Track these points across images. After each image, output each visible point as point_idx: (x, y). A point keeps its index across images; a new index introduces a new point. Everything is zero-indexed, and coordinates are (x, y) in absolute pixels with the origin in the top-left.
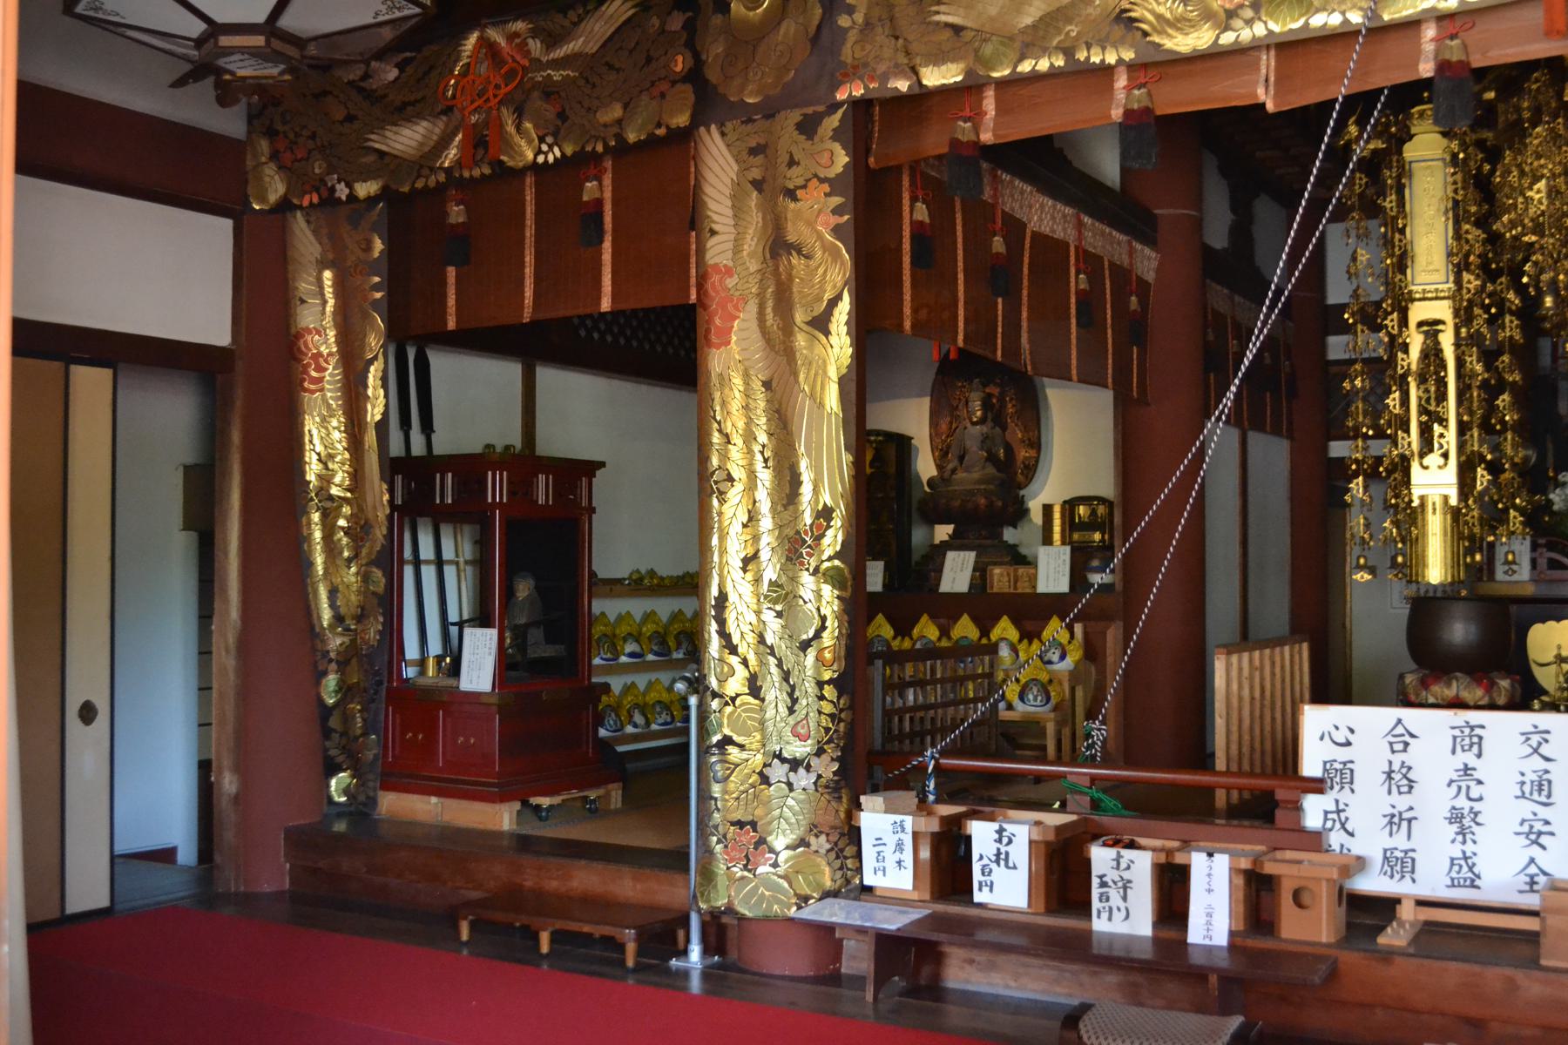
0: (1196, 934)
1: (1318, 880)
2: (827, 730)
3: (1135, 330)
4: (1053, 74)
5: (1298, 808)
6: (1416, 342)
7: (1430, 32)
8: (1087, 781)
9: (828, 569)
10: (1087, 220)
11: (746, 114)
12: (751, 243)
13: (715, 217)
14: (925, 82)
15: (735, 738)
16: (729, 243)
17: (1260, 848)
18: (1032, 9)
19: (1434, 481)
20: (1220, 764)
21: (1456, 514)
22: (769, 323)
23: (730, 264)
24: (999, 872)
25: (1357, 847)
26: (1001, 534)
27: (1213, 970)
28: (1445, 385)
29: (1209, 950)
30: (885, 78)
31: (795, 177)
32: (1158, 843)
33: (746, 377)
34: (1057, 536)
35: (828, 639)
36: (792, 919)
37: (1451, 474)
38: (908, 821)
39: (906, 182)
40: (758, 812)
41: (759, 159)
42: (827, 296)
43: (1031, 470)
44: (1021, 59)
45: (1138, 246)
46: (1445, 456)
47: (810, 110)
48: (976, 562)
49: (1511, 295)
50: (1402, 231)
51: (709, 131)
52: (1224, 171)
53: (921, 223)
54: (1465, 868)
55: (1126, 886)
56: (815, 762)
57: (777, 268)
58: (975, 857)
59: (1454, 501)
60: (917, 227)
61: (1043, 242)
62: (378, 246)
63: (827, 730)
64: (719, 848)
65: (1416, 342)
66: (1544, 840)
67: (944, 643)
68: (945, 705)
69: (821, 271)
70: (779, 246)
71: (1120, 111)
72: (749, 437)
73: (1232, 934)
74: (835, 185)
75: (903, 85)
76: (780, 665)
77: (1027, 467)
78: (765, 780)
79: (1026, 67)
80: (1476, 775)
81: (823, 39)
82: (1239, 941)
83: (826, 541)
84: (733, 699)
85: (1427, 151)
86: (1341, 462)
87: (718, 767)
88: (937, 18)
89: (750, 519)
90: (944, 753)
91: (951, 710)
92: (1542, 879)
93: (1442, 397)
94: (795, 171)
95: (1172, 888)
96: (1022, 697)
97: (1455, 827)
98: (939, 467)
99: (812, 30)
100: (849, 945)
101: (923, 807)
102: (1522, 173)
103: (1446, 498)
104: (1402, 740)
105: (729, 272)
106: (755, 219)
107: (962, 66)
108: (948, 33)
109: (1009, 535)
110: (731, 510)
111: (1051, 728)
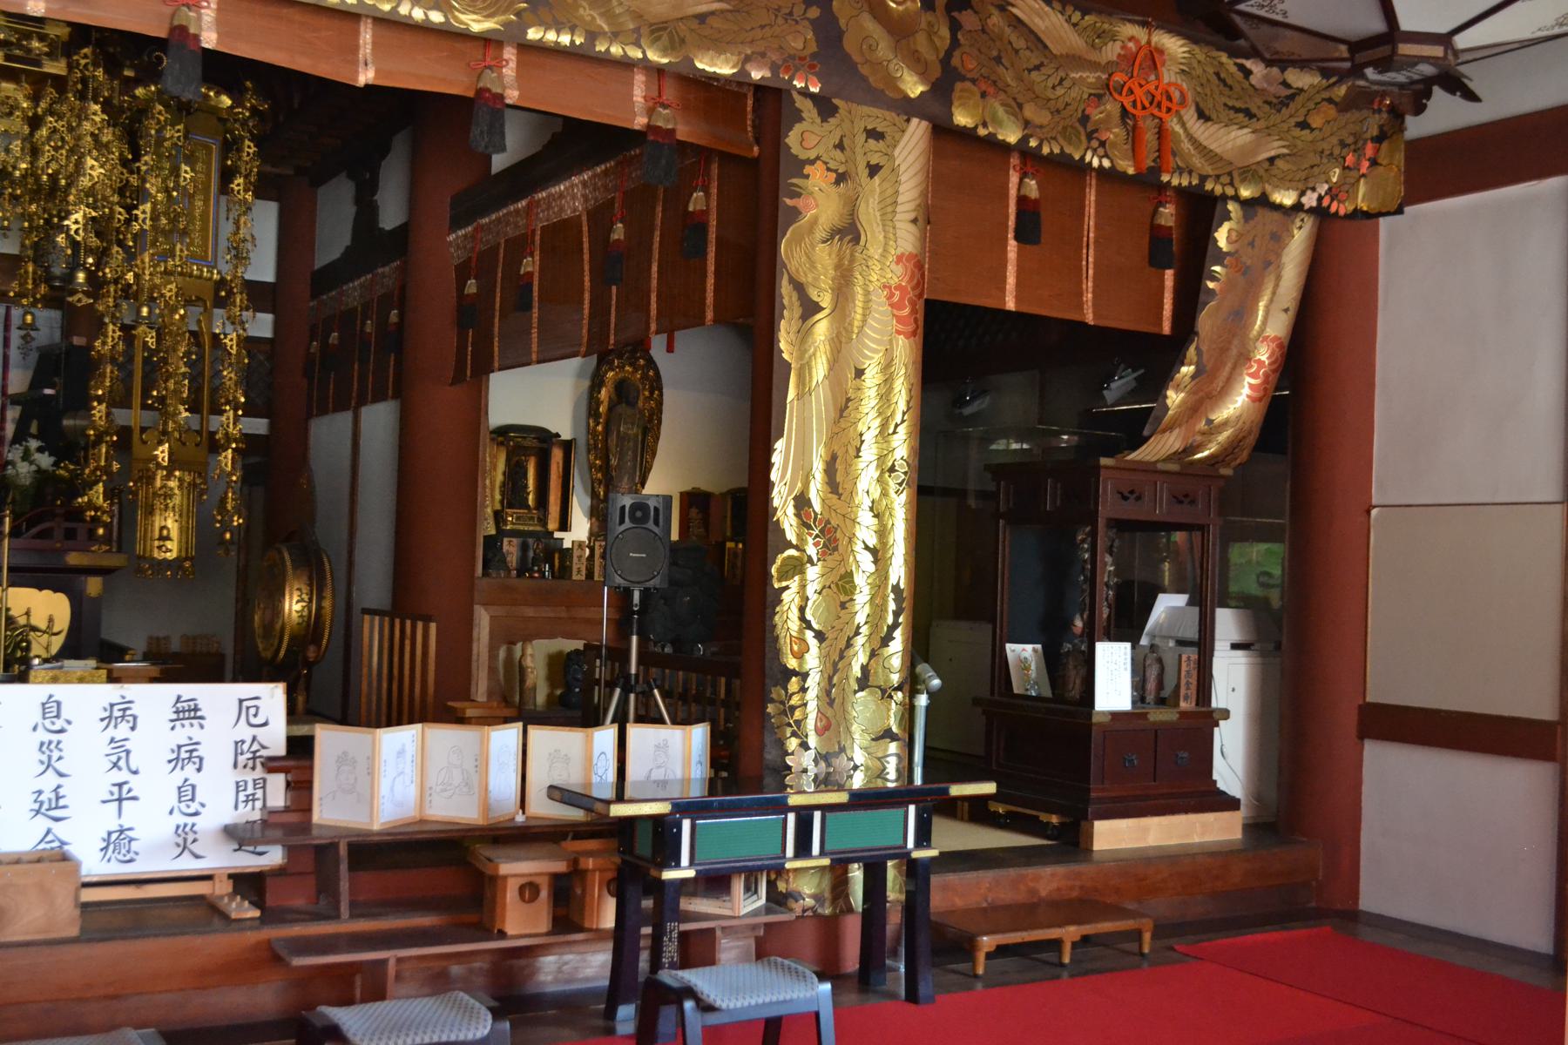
54: (118, 840)
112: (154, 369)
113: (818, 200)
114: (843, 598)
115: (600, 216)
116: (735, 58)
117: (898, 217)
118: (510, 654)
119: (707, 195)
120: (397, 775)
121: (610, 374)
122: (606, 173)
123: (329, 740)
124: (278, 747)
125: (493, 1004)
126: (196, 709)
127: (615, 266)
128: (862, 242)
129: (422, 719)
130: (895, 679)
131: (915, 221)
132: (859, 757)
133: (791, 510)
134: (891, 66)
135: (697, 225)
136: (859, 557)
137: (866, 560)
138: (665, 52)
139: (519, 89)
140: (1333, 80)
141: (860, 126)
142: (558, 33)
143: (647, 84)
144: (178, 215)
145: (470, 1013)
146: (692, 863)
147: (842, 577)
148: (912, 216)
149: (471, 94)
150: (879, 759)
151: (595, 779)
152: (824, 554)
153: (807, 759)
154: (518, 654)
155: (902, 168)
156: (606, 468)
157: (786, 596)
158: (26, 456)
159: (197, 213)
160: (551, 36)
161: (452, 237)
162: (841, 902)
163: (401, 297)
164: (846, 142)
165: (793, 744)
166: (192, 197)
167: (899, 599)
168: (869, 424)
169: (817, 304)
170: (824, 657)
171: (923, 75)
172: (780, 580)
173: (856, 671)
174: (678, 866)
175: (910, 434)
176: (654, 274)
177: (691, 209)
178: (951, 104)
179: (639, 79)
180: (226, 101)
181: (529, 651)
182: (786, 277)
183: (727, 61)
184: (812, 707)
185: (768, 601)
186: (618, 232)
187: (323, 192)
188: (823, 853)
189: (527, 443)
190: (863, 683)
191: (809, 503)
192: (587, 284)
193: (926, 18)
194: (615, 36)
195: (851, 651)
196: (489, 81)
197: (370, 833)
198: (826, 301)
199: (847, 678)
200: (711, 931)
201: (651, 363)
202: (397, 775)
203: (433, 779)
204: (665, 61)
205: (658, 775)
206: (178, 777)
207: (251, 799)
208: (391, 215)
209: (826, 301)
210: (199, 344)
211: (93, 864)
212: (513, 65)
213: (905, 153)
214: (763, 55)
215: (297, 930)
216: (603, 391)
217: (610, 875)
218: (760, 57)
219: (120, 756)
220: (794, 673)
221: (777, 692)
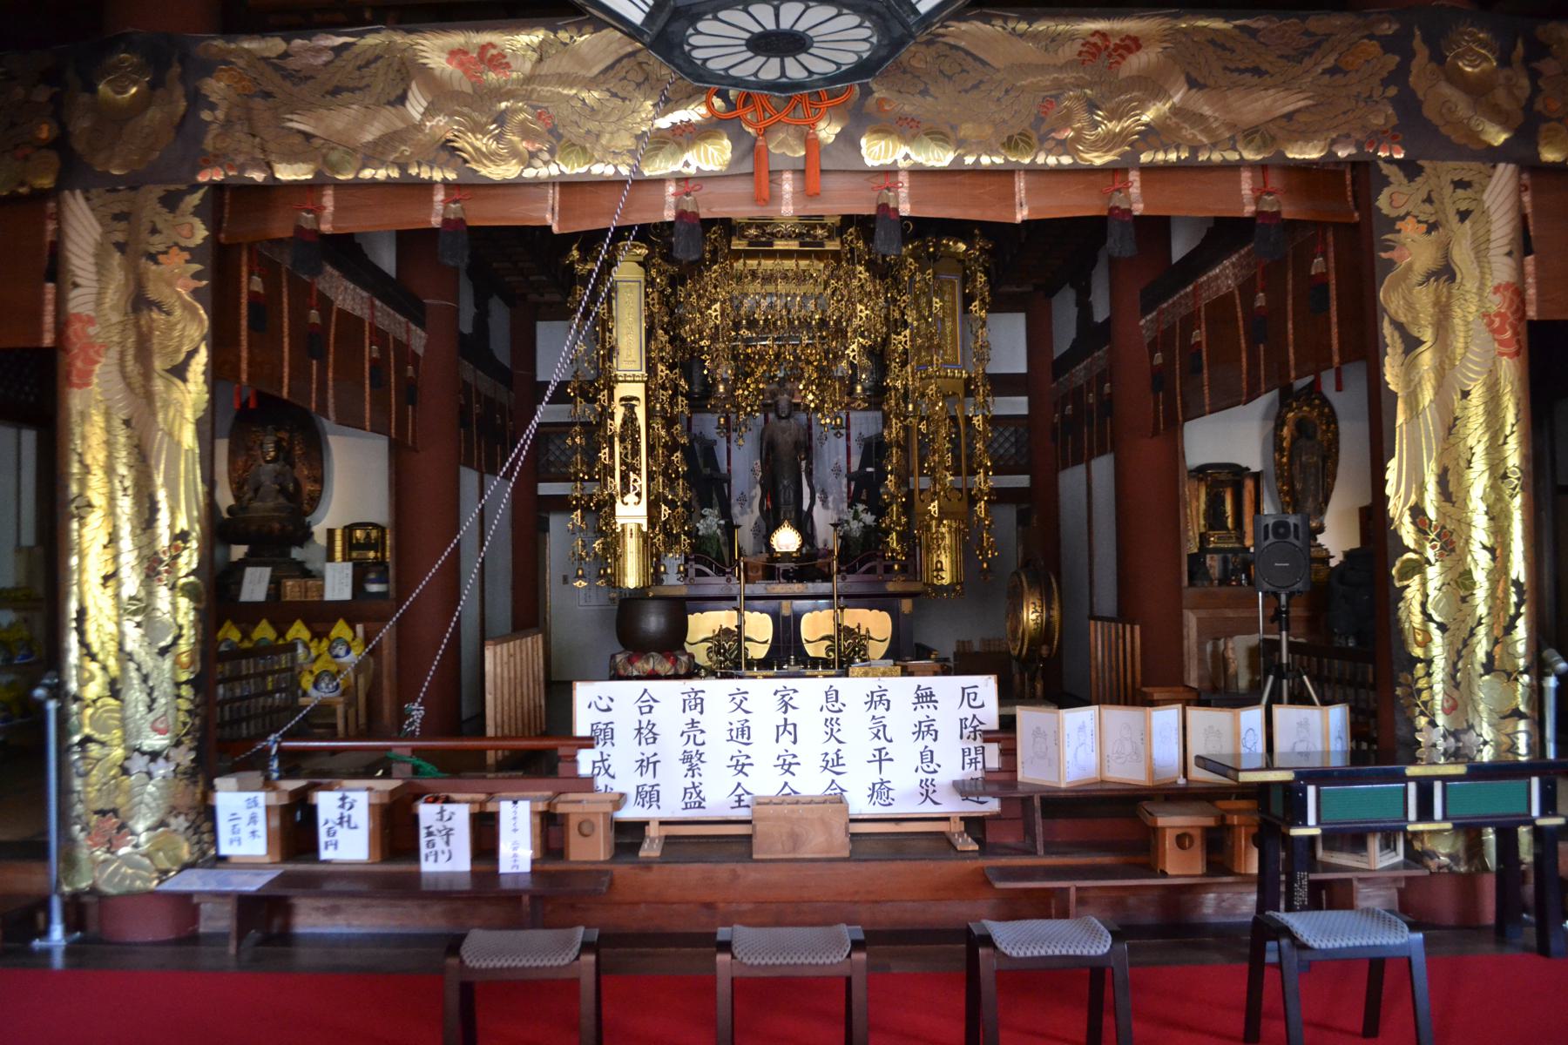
0: (505, 866)
1: (597, 814)
2: (185, 724)
3: (410, 392)
4: (388, 184)
5: (573, 760)
6: (619, 412)
7: (671, 189)
8: (408, 752)
9: (185, 585)
10: (378, 303)
11: (112, 184)
12: (112, 296)
14: (278, 176)
15: (97, 736)
16: (92, 292)
17: (549, 793)
18: (373, 129)
20: (490, 731)
21: (646, 539)
22: (129, 369)
23: (93, 314)
24: (343, 833)
25: (618, 786)
26: (289, 554)
27: (524, 891)
28: (638, 444)
29: (516, 876)
30: (242, 168)
31: (157, 244)
32: (468, 796)
33: (108, 416)
34: (338, 555)
35: (184, 646)
36: (153, 893)
38: (261, 797)
39: (245, 258)
40: (120, 800)
41: (123, 225)
42: (185, 349)
43: (315, 501)
44: (364, 167)
45: (413, 327)
46: (639, 495)
47: (172, 187)
48: (272, 576)
49: (682, 382)
50: (610, 331)
53: (257, 293)
54: (694, 796)
55: (448, 833)
56: (173, 753)
58: (321, 821)
59: (645, 529)
60: (253, 295)
61: (343, 314)
63: (185, 724)
64: (82, 836)
65: (619, 412)
66: (746, 769)
67: (247, 644)
68: (257, 695)
69: (179, 327)
70: (140, 302)
71: (439, 219)
72: (110, 470)
73: (533, 862)
74: (195, 254)
75: (258, 176)
76: (139, 669)
77: (312, 499)
78: (125, 771)
79: (367, 174)
80: (700, 726)
81: (187, 128)
82: (538, 866)
83: (182, 561)
84: (94, 701)
85: (628, 273)
87: (80, 763)
88: (290, 124)
89: (110, 541)
90: (285, 737)
91: (261, 700)
92: (745, 797)
93: (636, 452)
94: (156, 239)
95: (485, 831)
96: (316, 685)
97: (687, 766)
98: (237, 497)
99: (177, 119)
100: (206, 908)
101: (268, 785)
102: (700, 297)
103: (639, 526)
104: (648, 705)
105: (91, 321)
107: (312, 167)
108: (298, 139)
109: (296, 553)
110: (90, 535)
111: (340, 710)
112: (925, 446)
113: (1413, 250)
114: (1462, 593)
118: (1215, 647)
119: (1326, 259)
120: (1079, 745)
121: (1291, 415)
122: (1249, 254)
123: (1029, 718)
124: (993, 724)
125: (1116, 928)
126: (932, 695)
127: (1263, 327)
129: (1097, 703)
130: (1522, 662)
131: (1509, 254)
132: (1487, 732)
133: (1407, 519)
134: (1473, 122)
135: (1321, 283)
138: (1258, 150)
139: (1144, 201)
140: (694, 113)
142: (1166, 152)
143: (1253, 178)
144: (933, 335)
145: (1094, 932)
146: (1319, 823)
147: (1461, 575)
148: (1507, 249)
149: (1105, 213)
150: (1508, 735)
151: (1243, 750)
152: (1441, 555)
153: (1437, 736)
154: (1222, 647)
155: (1493, 209)
156: (1292, 492)
157: (1409, 593)
158: (856, 517)
159: (948, 330)
160: (1160, 156)
161: (1142, 323)
162: (1476, 861)
164: (1434, 195)
165: (1422, 721)
166: (943, 320)
167: (1520, 593)
168: (1475, 437)
170: (1449, 645)
171: (1504, 124)
174: (1305, 825)
175: (1521, 443)
176: (1290, 331)
178: (1537, 144)
180: (962, 247)
181: (1230, 645)
182: (1386, 320)
183: (1315, 147)
184: (1438, 688)
188: (1445, 818)
189: (1222, 477)
190: (1489, 667)
191: (1423, 512)
192: (1243, 345)
193: (1507, 72)
194: (1214, 146)
195: (1475, 640)
196: (1118, 200)
197: (1060, 790)
198: (1427, 335)
200: (1349, 881)
201: (1325, 402)
202: (1079, 745)
203: (1110, 749)
204: (1259, 157)
205: (1301, 747)
206: (920, 745)
207: (974, 762)
208: (1101, 314)
209: (1427, 335)
210: (957, 425)
211: (859, 804)
212: (1137, 184)
214: (1348, 136)
215: (1004, 861)
216: (1285, 430)
217: (1255, 830)
218: (1344, 139)
219: (880, 731)
220: (1419, 660)
221: (1403, 677)
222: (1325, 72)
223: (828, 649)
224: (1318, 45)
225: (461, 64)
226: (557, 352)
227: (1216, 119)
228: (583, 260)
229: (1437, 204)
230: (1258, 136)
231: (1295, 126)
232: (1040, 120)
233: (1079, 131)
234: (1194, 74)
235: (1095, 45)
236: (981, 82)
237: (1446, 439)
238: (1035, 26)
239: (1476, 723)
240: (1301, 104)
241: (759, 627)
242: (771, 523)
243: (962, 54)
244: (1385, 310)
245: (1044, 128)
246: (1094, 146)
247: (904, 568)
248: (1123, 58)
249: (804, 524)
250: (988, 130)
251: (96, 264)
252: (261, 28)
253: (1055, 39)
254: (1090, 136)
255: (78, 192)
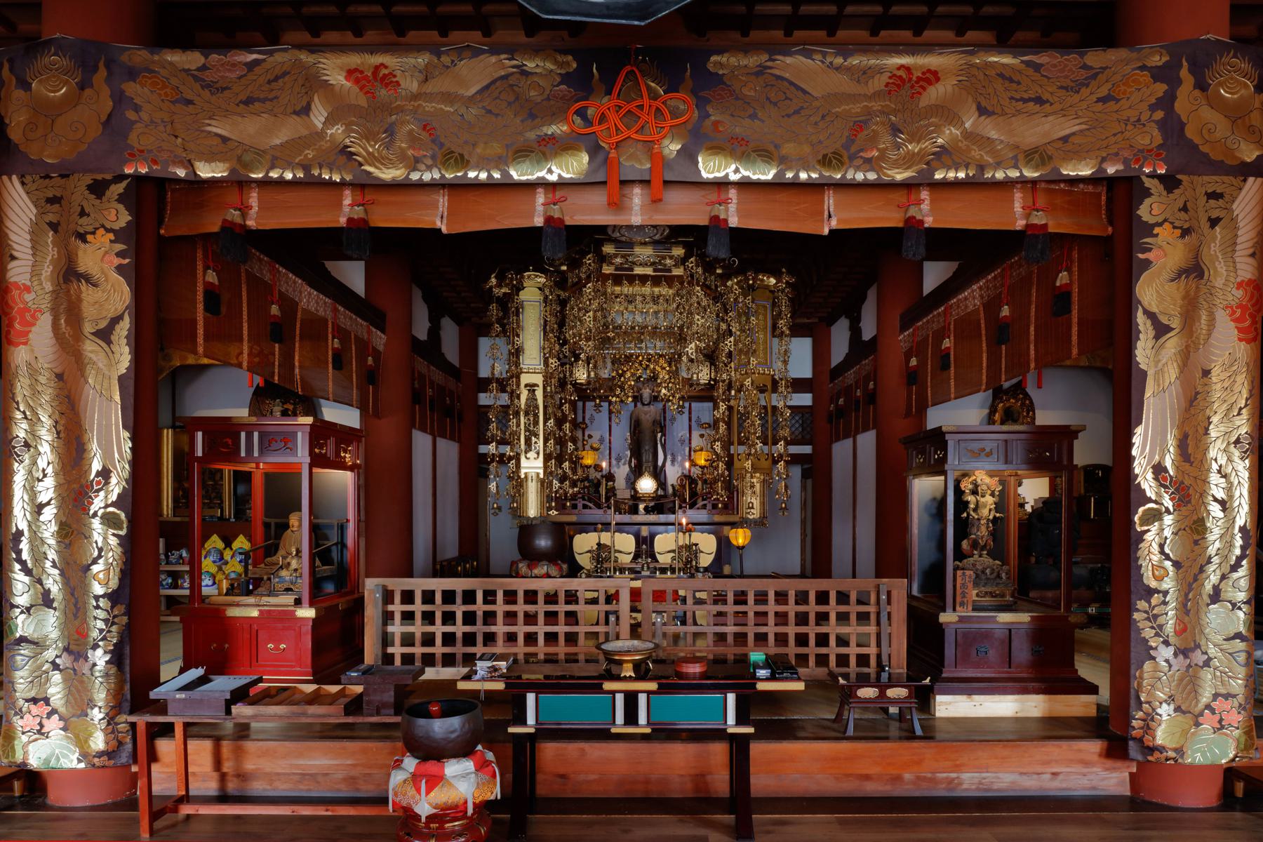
4: (294, 183)
10: (341, 309)
12: (47, 270)
13: (15, 246)
19: (532, 465)
21: (542, 482)
23: (29, 283)
31: (85, 224)
37: (540, 463)
44: (272, 167)
46: (538, 453)
47: (99, 177)
50: (518, 336)
51: (10, 179)
52: (425, 299)
57: (69, 291)
62: (493, 486)
70: (69, 275)
74: (119, 236)
75: (181, 173)
86: (485, 455)
88: (209, 128)
93: (536, 423)
94: (84, 220)
99: (104, 118)
102: (580, 309)
105: (28, 289)
106: (51, 252)
107: (227, 165)
108: (219, 140)
113: (1164, 253)
114: (1196, 537)
115: (991, 306)
116: (1093, 162)
117: (1237, 254)
127: (1001, 333)
128: (1206, 277)
131: (1253, 255)
133: (1150, 476)
136: (1210, 508)
137: (1215, 509)
138: (1036, 168)
141: (1201, 191)
143: (1023, 198)
147: (1195, 522)
148: (1251, 251)
152: (1179, 506)
155: (1240, 218)
157: (1148, 537)
163: (874, 375)
169: (1168, 326)
172: (1141, 525)
173: (1208, 587)
175: (1252, 415)
177: (1058, 284)
179: (1018, 196)
180: (773, 281)
182: (1140, 309)
185: (1130, 541)
186: (1005, 311)
187: (833, 328)
194: (998, 165)
195: (1204, 575)
199: (1200, 595)
201: (1027, 396)
204: (1036, 175)
213: (1243, 205)
222: (1099, 100)
223: (673, 559)
224: (1094, 77)
225: (357, 81)
226: (490, 361)
227: (1002, 142)
228: (499, 285)
229: (1191, 212)
230: (1037, 156)
231: (1068, 147)
232: (851, 141)
233: (883, 152)
234: (984, 104)
235: (900, 77)
236: (802, 108)
237: (1187, 410)
238: (849, 60)
239: (1203, 642)
240: (1076, 128)
241: (625, 543)
242: (637, 473)
243: (786, 84)
244: (1139, 302)
245: (853, 150)
246: (896, 165)
247: (726, 506)
248: (924, 89)
249: (658, 475)
250: (807, 149)
251: (31, 240)
252: (185, 45)
253: (866, 74)
254: (893, 155)
255: (14, 177)
